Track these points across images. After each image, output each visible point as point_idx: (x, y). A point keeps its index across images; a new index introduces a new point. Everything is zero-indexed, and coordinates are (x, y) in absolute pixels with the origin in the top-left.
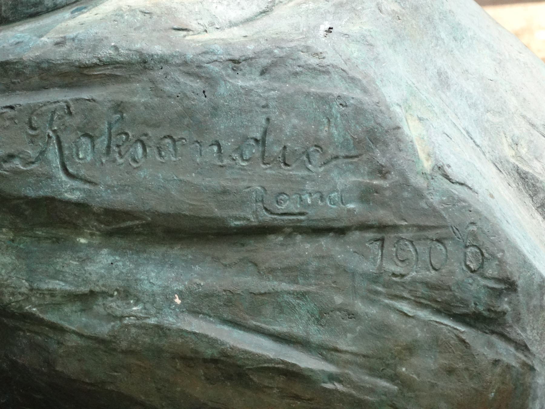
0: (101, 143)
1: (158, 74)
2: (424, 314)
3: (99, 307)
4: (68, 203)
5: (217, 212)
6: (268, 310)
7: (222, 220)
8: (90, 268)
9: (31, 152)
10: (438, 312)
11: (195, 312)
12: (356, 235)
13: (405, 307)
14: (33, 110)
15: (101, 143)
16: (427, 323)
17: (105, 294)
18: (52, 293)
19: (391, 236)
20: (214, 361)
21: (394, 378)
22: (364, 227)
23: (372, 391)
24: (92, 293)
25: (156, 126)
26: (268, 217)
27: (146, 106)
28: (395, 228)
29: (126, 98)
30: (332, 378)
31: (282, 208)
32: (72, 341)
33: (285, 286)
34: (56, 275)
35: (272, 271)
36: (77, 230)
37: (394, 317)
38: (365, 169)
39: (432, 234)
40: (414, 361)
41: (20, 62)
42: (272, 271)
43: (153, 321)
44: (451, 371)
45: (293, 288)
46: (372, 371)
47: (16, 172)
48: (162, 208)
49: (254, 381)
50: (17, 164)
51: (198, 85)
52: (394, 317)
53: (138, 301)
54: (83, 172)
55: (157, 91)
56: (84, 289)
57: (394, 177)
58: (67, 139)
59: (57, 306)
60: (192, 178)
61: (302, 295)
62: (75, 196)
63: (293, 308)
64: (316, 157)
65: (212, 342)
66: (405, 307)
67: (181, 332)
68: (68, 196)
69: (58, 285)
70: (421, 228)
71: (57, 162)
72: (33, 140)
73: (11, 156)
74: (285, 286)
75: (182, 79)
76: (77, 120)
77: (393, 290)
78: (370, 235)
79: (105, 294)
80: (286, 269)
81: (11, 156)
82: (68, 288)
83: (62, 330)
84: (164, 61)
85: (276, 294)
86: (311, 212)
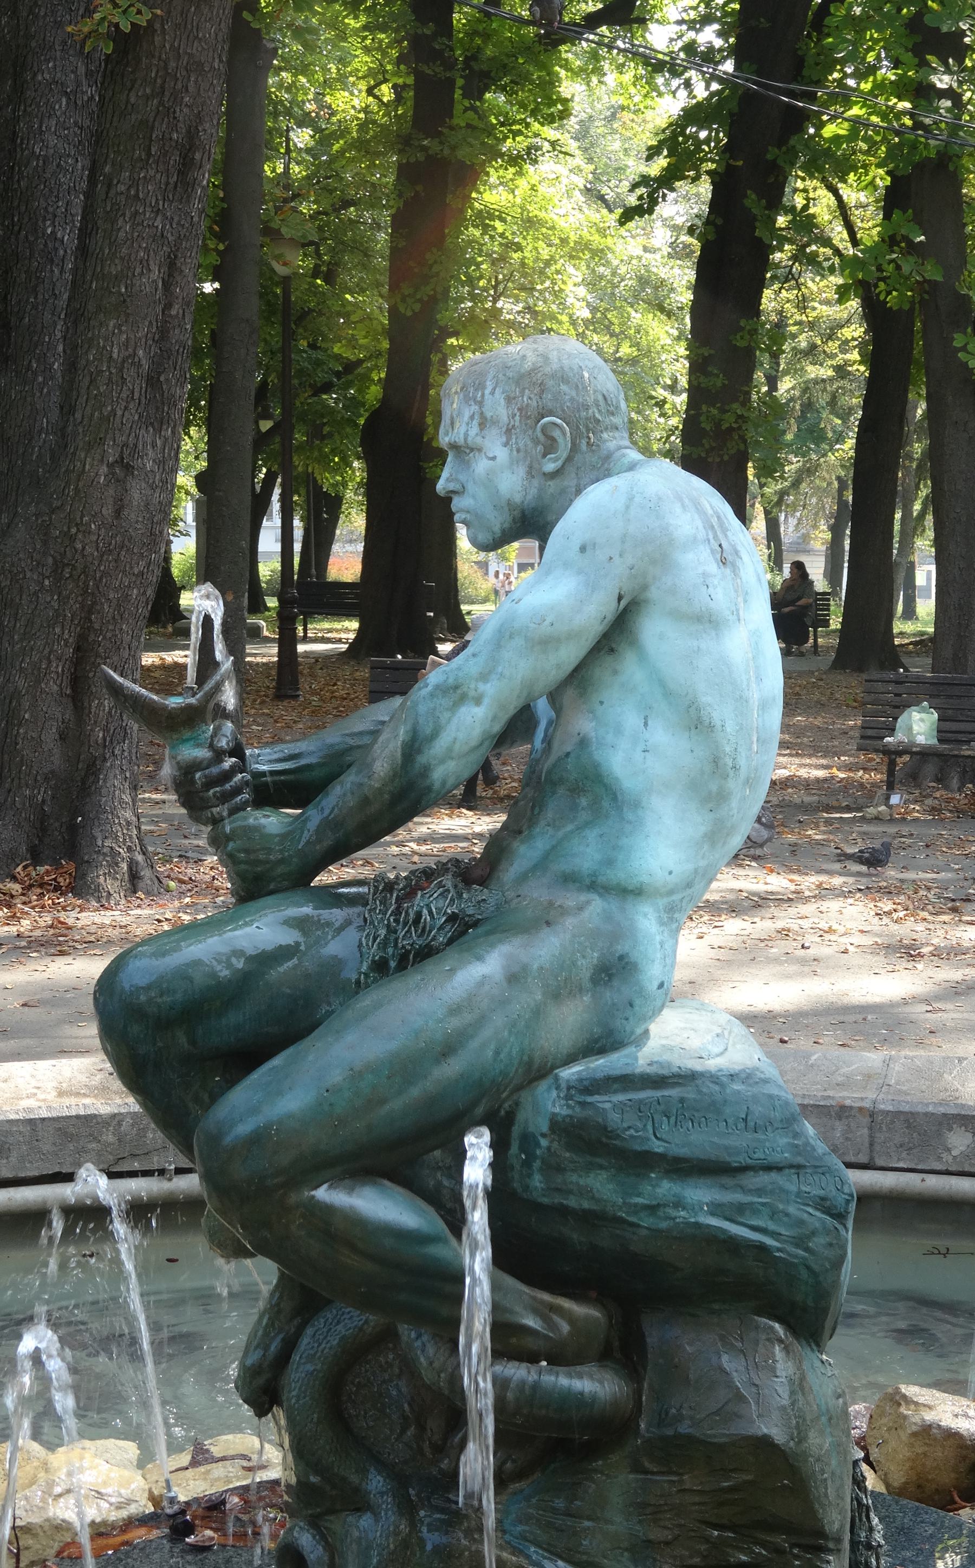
0: (673, 1120)
1: (699, 1082)
2: (818, 1214)
3: (660, 1213)
4: (657, 1154)
5: (728, 1159)
6: (747, 1213)
7: (729, 1163)
8: (659, 1190)
9: (640, 1125)
10: (824, 1212)
11: (713, 1214)
12: (787, 1171)
13: (811, 1211)
14: (641, 1101)
15: (673, 1120)
16: (820, 1219)
17: (665, 1205)
18: (636, 1205)
19: (802, 1172)
20: (724, 1241)
21: (807, 1249)
22: (791, 1166)
23: (796, 1256)
24: (659, 1205)
25: (698, 1111)
26: (750, 1161)
27: (695, 1100)
28: (804, 1167)
29: (686, 1095)
30: (779, 1250)
31: (756, 1156)
32: (644, 1232)
33: (756, 1200)
34: (639, 1195)
35: (750, 1191)
36: (652, 1168)
37: (805, 1216)
38: (791, 1135)
39: (820, 1170)
40: (815, 1239)
41: (634, 1075)
42: (750, 1191)
43: (693, 1220)
44: (831, 1245)
45: (760, 1200)
46: (797, 1246)
47: (632, 1136)
48: (702, 1157)
49: (211, 1529)
50: (632, 1132)
51: (717, 1088)
52: (805, 1216)
53: (684, 1209)
54: (664, 1136)
55: (700, 1092)
56: (654, 1203)
57: (803, 1139)
58: (656, 1117)
59: (636, 1213)
60: (716, 1140)
61: (763, 1204)
62: (660, 1150)
63: (759, 1211)
64: (769, 1129)
65: (724, 1231)
66: (811, 1211)
67: (708, 1226)
68: (656, 1150)
69: (639, 1200)
70: (816, 1167)
71: (651, 1131)
72: (640, 1118)
73: (629, 1128)
74: (756, 1200)
75: (711, 1085)
76: (662, 1107)
77: (413, 1335)
78: (793, 1171)
79: (665, 1205)
80: (758, 1190)
81: (629, 1128)
82: (646, 1202)
83: (638, 1226)
84: (702, 1074)
85: (752, 1203)
86: (769, 1158)
